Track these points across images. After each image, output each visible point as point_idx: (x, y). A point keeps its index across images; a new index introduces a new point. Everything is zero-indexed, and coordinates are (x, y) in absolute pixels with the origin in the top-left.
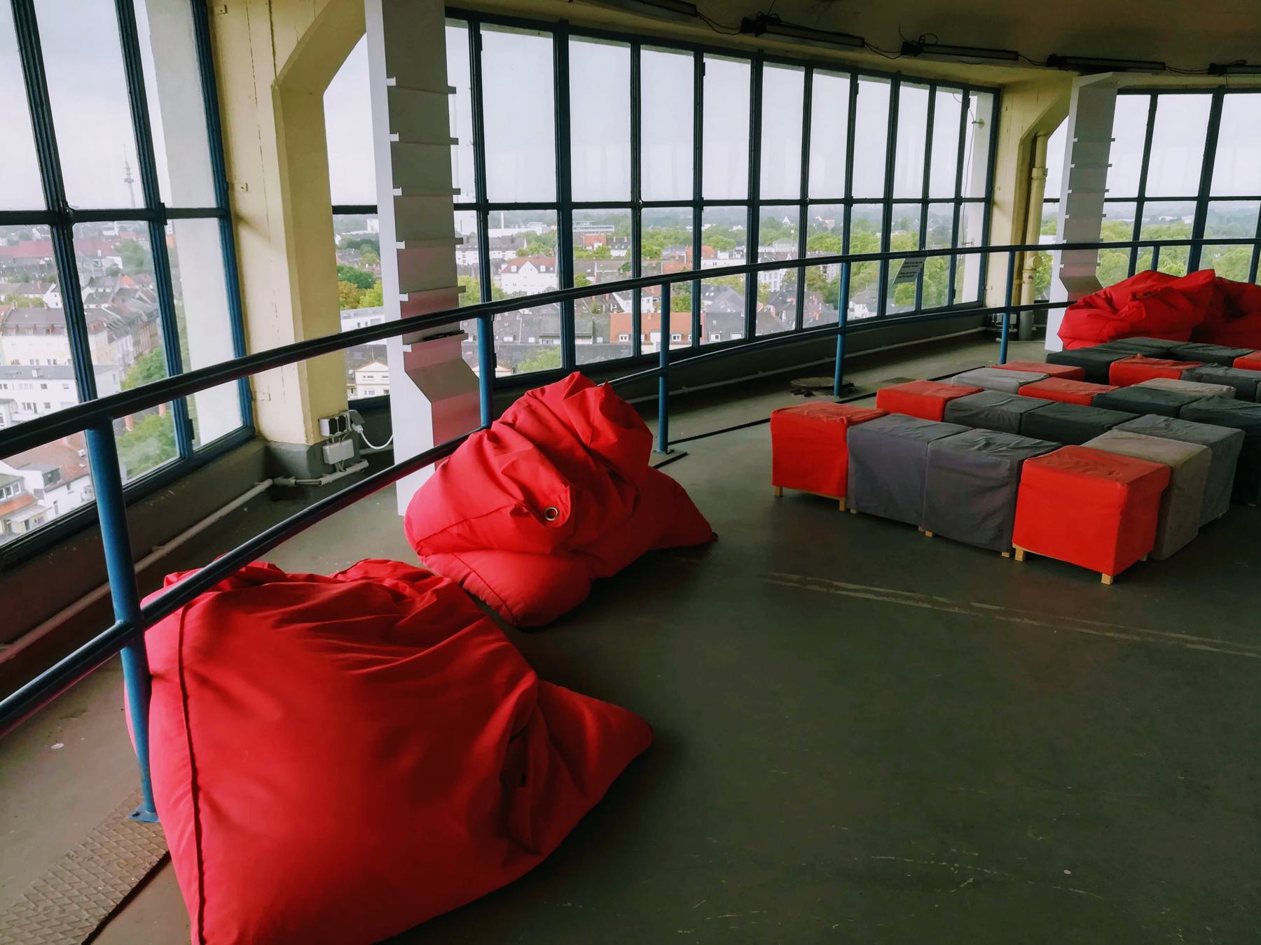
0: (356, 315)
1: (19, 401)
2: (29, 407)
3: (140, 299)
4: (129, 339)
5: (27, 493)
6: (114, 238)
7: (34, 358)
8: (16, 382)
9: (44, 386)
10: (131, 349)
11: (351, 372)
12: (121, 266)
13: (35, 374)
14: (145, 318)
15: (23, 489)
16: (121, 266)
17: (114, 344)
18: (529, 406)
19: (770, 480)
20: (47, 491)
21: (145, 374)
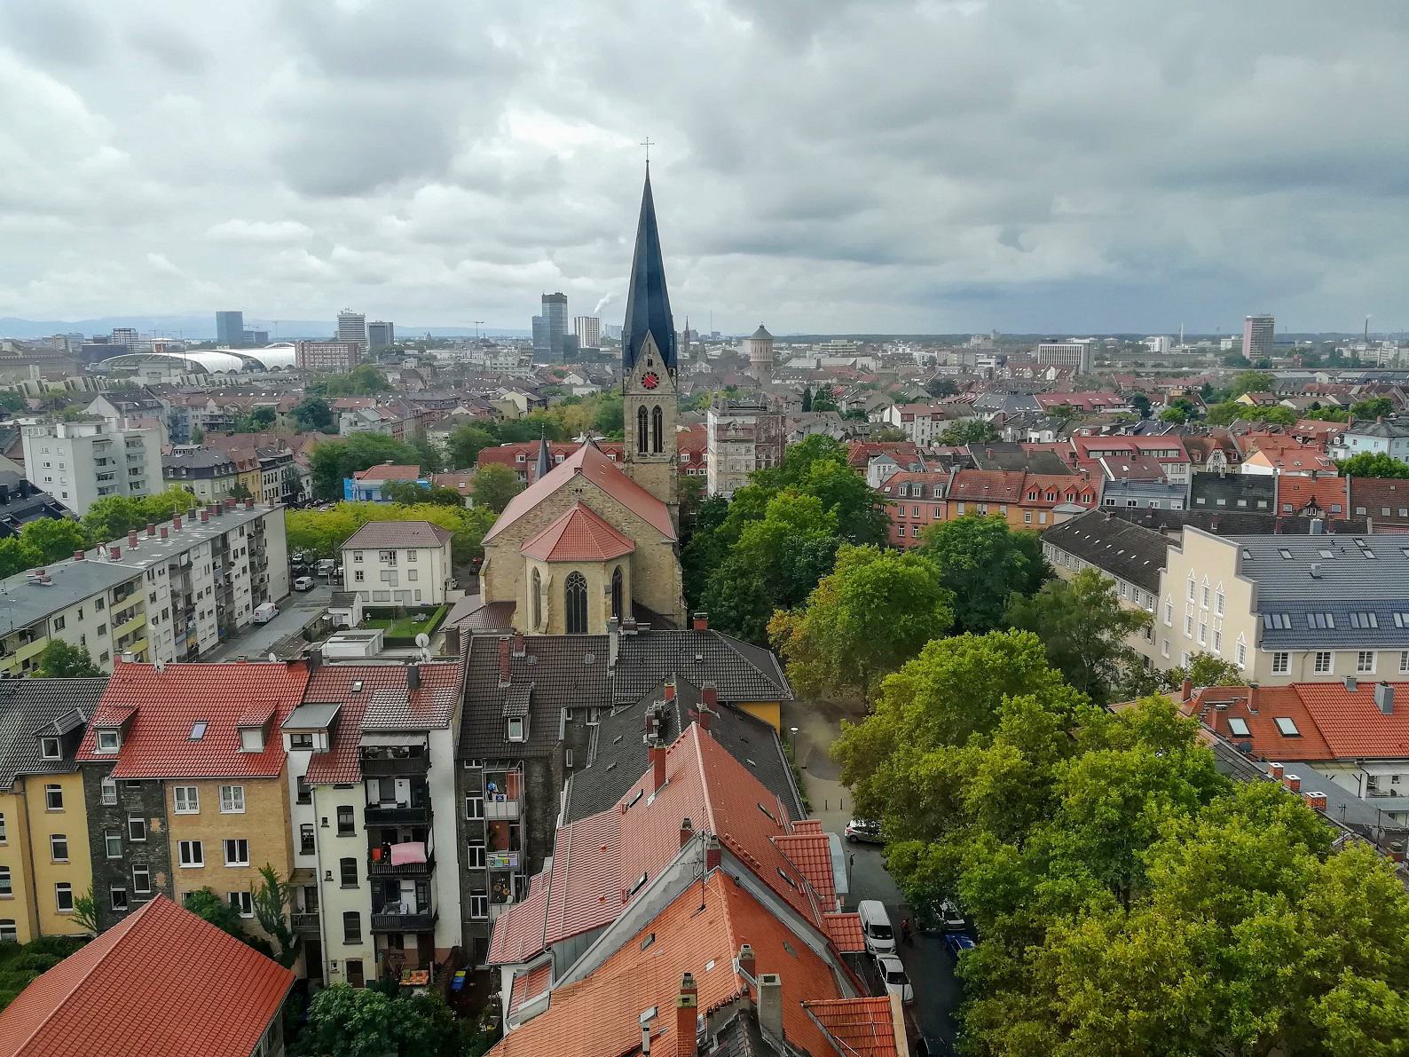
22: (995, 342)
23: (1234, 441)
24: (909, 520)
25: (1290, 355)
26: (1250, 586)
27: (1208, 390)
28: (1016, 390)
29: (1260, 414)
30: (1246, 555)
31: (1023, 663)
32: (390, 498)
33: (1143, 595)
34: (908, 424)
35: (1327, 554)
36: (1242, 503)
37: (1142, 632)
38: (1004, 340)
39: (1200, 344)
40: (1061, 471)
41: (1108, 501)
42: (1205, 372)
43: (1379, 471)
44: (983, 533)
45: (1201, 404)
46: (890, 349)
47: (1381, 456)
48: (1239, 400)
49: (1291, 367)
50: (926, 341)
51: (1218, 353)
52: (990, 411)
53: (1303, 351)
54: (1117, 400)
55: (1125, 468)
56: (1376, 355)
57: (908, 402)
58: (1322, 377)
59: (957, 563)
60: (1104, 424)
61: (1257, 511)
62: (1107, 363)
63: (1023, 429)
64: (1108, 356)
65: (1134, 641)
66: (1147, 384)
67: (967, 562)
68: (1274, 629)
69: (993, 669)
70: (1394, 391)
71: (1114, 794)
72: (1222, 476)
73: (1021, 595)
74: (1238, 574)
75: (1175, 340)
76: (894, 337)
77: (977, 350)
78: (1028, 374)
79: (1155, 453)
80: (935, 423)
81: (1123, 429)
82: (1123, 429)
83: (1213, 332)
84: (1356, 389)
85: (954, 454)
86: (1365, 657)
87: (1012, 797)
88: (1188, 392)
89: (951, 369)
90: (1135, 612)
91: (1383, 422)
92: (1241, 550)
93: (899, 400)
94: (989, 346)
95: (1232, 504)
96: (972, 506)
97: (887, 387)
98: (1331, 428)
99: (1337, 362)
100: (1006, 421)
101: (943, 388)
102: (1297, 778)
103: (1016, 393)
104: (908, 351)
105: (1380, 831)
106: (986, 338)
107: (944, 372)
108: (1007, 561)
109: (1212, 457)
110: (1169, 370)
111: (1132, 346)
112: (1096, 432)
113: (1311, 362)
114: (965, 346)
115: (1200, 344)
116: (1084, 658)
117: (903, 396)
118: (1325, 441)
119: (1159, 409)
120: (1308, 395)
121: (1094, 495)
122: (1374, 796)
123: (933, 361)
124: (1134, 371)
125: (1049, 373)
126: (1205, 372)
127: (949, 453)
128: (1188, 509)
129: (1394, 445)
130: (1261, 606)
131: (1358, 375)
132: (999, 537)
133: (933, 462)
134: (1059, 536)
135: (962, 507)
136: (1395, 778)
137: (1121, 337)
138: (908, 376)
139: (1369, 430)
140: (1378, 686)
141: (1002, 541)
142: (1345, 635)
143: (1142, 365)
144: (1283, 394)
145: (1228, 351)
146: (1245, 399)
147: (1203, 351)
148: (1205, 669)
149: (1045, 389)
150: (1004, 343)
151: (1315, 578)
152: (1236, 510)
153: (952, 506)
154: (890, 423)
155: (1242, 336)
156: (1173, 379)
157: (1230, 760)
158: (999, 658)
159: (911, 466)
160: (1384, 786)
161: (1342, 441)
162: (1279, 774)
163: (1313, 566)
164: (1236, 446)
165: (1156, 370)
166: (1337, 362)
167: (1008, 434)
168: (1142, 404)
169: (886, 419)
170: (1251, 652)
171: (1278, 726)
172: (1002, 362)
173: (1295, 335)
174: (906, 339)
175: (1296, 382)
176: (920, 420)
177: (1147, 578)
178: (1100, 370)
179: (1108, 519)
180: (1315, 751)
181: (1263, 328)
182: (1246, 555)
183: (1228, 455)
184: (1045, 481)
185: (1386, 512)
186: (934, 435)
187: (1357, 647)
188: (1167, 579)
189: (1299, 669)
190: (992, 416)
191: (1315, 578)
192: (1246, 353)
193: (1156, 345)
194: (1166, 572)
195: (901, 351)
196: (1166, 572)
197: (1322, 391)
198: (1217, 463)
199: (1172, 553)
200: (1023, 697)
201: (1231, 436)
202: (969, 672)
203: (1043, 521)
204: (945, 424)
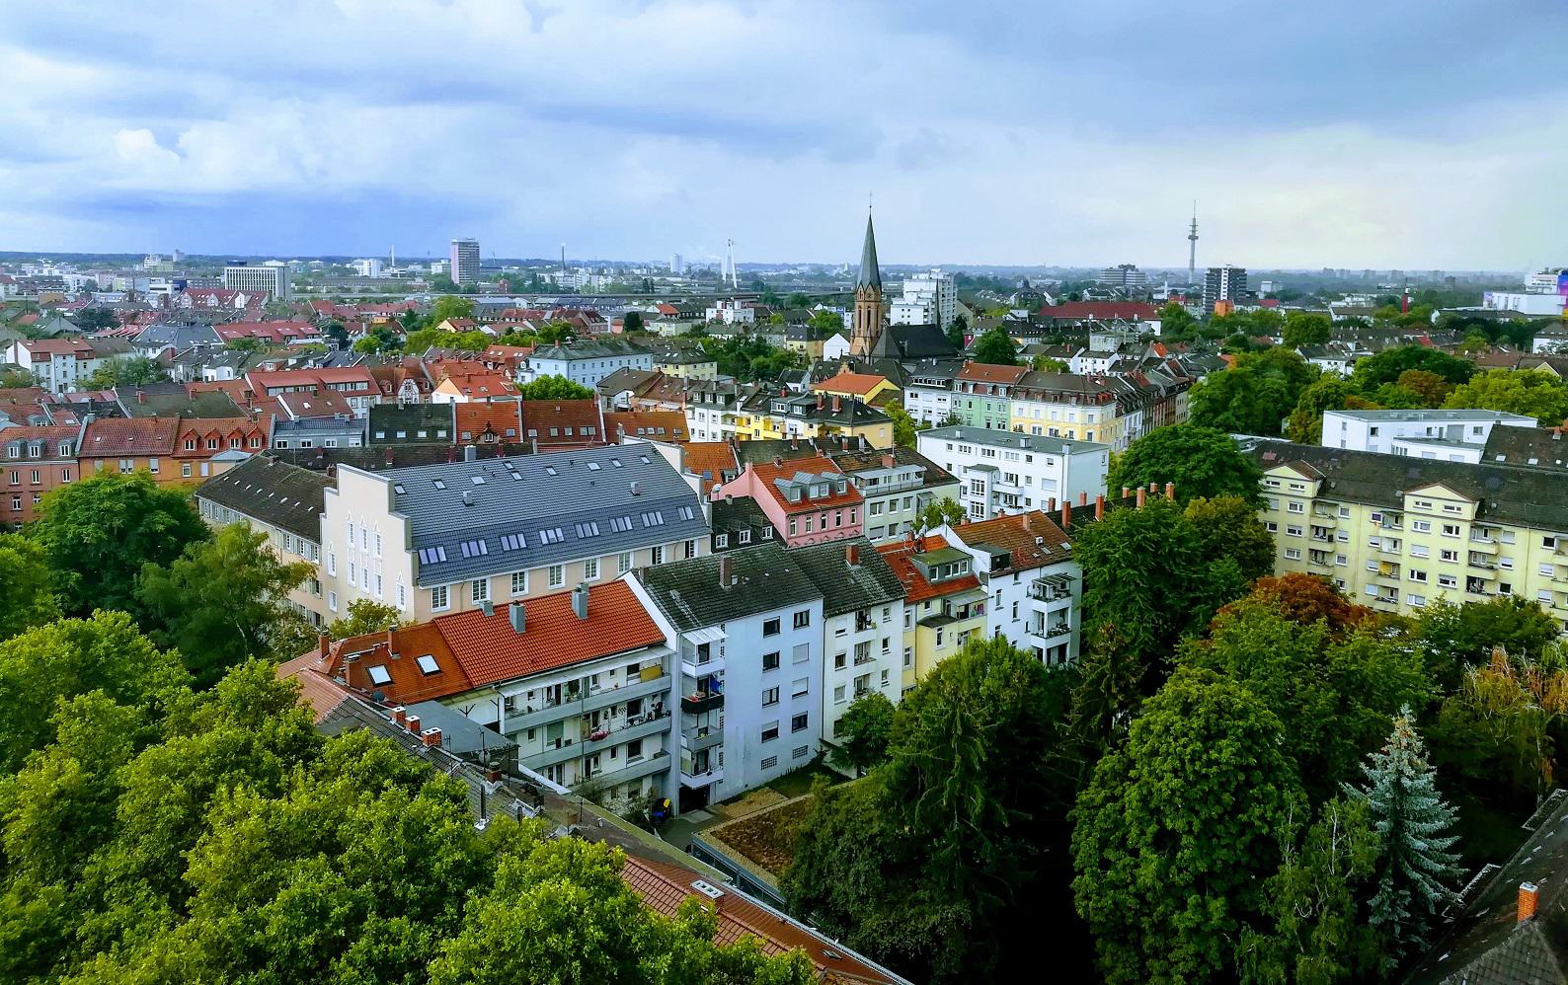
0: (1427, 418)
1: (1003, 471)
2: (1011, 479)
3: (1163, 371)
4: (1139, 415)
5: (973, 576)
6: (1163, 301)
7: (1055, 428)
8: (1004, 450)
9: (1029, 459)
10: (1139, 427)
11: (1399, 493)
12: (1158, 333)
13: (1023, 443)
14: (1163, 392)
15: (970, 569)
16: (1158, 333)
17: (1121, 419)
18: (1331, 539)
19: (403, 547)
20: (993, 577)
21: (1132, 460)
22: (177, 263)
23: (425, 370)
24: (26, 487)
25: (496, 281)
26: (403, 522)
27: (411, 316)
28: (193, 320)
29: (453, 340)
30: (400, 490)
31: (102, 652)
32: (798, 411)
33: (307, 544)
34: (43, 366)
35: (478, 480)
36: (422, 434)
37: (306, 585)
38: (190, 262)
39: (411, 268)
40: (234, 413)
41: (279, 443)
42: (410, 298)
43: (557, 392)
44: (110, 496)
45: (403, 332)
46: (30, 270)
47: (558, 378)
48: (441, 327)
49: (495, 293)
50: (82, 261)
51: (427, 277)
52: (155, 346)
53: (507, 276)
54: (311, 329)
55: (307, 405)
56: (572, 282)
57: (47, 337)
58: (522, 303)
59: (79, 536)
60: (290, 356)
61: (437, 441)
62: (309, 288)
63: (198, 366)
64: (311, 280)
65: (300, 596)
66: (349, 310)
67: (89, 534)
68: (430, 564)
69: (57, 667)
70: (580, 315)
71: (178, 788)
72: (401, 408)
73: (156, 566)
74: (390, 511)
75: (386, 262)
76: (38, 255)
77: (152, 274)
78: (212, 301)
79: (341, 388)
80: (81, 363)
81: (311, 362)
82: (311, 362)
83: (425, 256)
84: (548, 315)
85: (92, 401)
86: (518, 578)
87: (67, 825)
88: (392, 319)
89: (114, 291)
90: (295, 565)
91: (560, 345)
92: (392, 486)
93: (33, 335)
94: (169, 268)
95: (412, 436)
96: (110, 463)
97: (14, 319)
98: (518, 353)
99: (538, 287)
100: (174, 357)
101: (96, 319)
102: (416, 718)
103: (192, 324)
104: (56, 273)
105: (486, 753)
106: (166, 259)
107: (101, 298)
108: (147, 525)
109: (403, 388)
110: (375, 296)
111: (339, 268)
112: (281, 366)
113: (516, 288)
114: (138, 268)
115: (411, 268)
116: (228, 628)
117: (39, 331)
118: (512, 364)
119: (357, 338)
120: (507, 320)
121: (221, 438)
122: (513, 717)
123: (91, 287)
124: (338, 297)
125: (237, 300)
126: (410, 298)
127: (85, 400)
128: (367, 446)
129: (571, 366)
130: (416, 541)
131: (552, 301)
132: (133, 498)
133: (64, 411)
134: (217, 490)
135: (98, 464)
136: (531, 694)
137: (328, 260)
138: (52, 305)
139: (550, 353)
140: (573, 594)
141: (139, 502)
142: (500, 560)
143: (348, 291)
144: (485, 319)
145: (437, 275)
146: (445, 325)
147: (413, 275)
148: (366, 619)
149: (228, 319)
150: (189, 265)
151: (467, 505)
152: (402, 442)
153: (85, 465)
154: (16, 365)
155: (450, 260)
156: (375, 305)
157: (358, 714)
158: (65, 650)
159: (31, 419)
160: (521, 705)
161: (528, 366)
162: (401, 717)
163: (465, 493)
164: (427, 374)
165: (361, 296)
166: (538, 287)
167: (177, 373)
168: (339, 333)
169: (10, 359)
170: (410, 590)
171: (371, 676)
172: (181, 286)
173: (501, 261)
174: (56, 259)
175: (495, 307)
176: (60, 360)
177: (307, 525)
178: (300, 296)
179: (271, 465)
180: (454, 682)
181: (469, 252)
182: (400, 490)
183: (419, 384)
184: (203, 426)
185: (554, 432)
186: (82, 377)
187: (583, 556)
188: (327, 524)
189: (458, 599)
190: (159, 352)
191: (467, 505)
192: (456, 279)
193: (365, 268)
194: (325, 517)
195: (46, 273)
196: (325, 517)
197: (520, 316)
198: (409, 393)
199: (329, 495)
200: (86, 695)
201: (422, 365)
202: (27, 676)
203: (205, 473)
204: (95, 364)
